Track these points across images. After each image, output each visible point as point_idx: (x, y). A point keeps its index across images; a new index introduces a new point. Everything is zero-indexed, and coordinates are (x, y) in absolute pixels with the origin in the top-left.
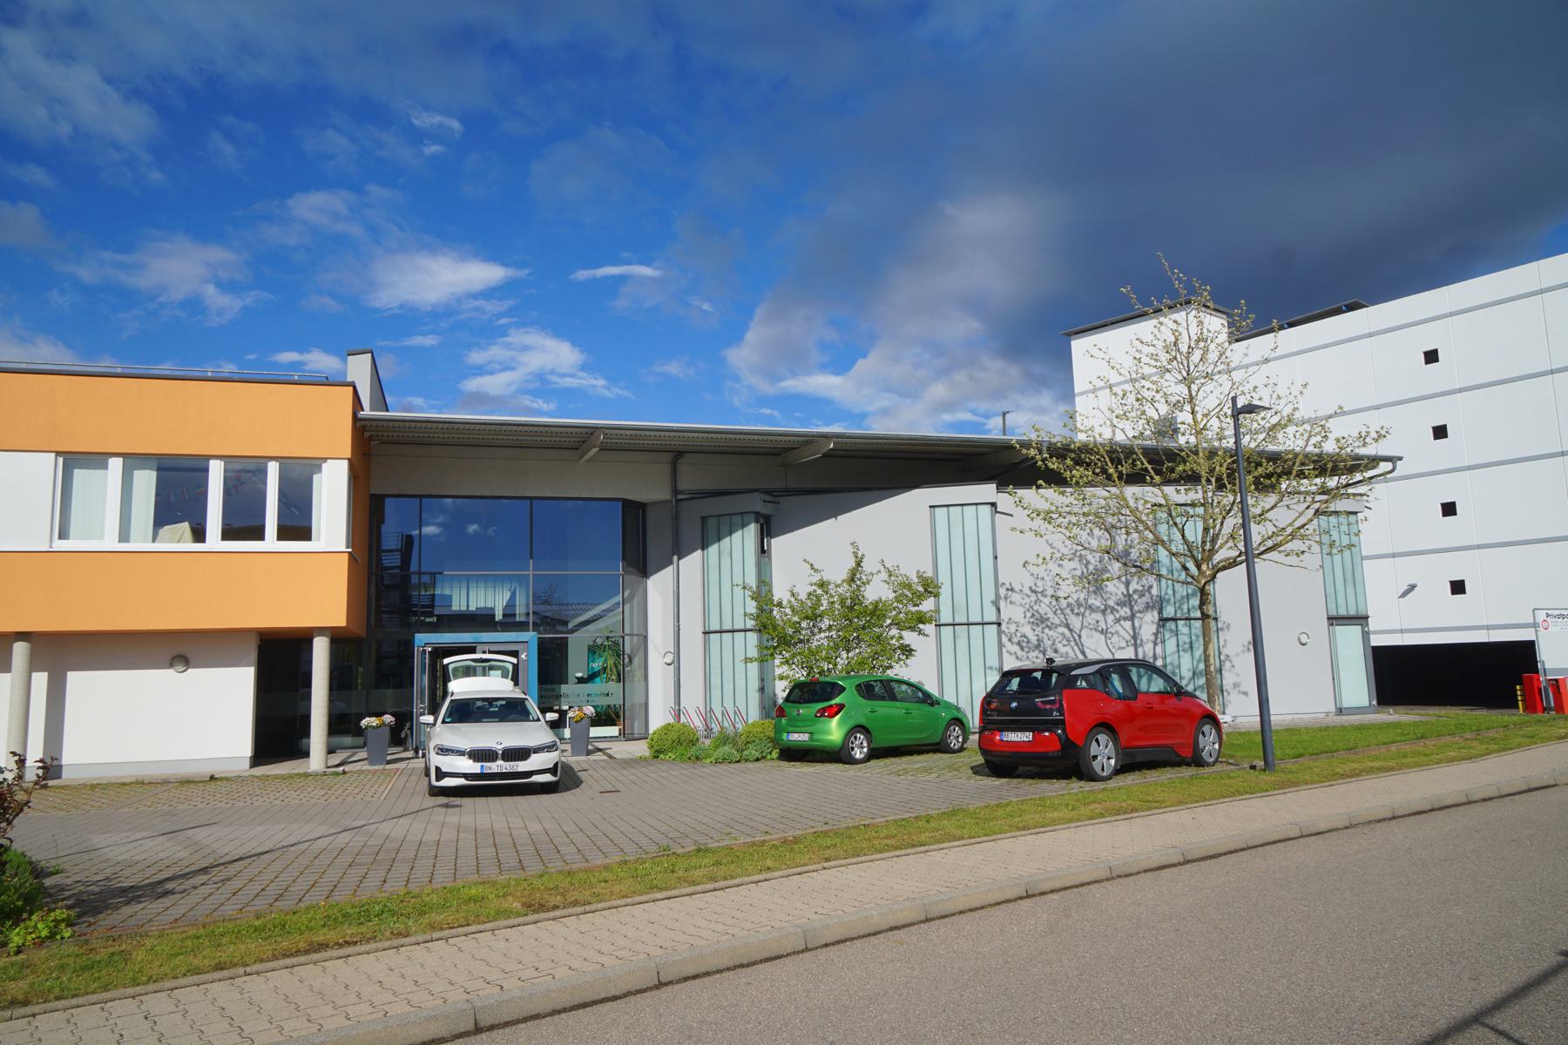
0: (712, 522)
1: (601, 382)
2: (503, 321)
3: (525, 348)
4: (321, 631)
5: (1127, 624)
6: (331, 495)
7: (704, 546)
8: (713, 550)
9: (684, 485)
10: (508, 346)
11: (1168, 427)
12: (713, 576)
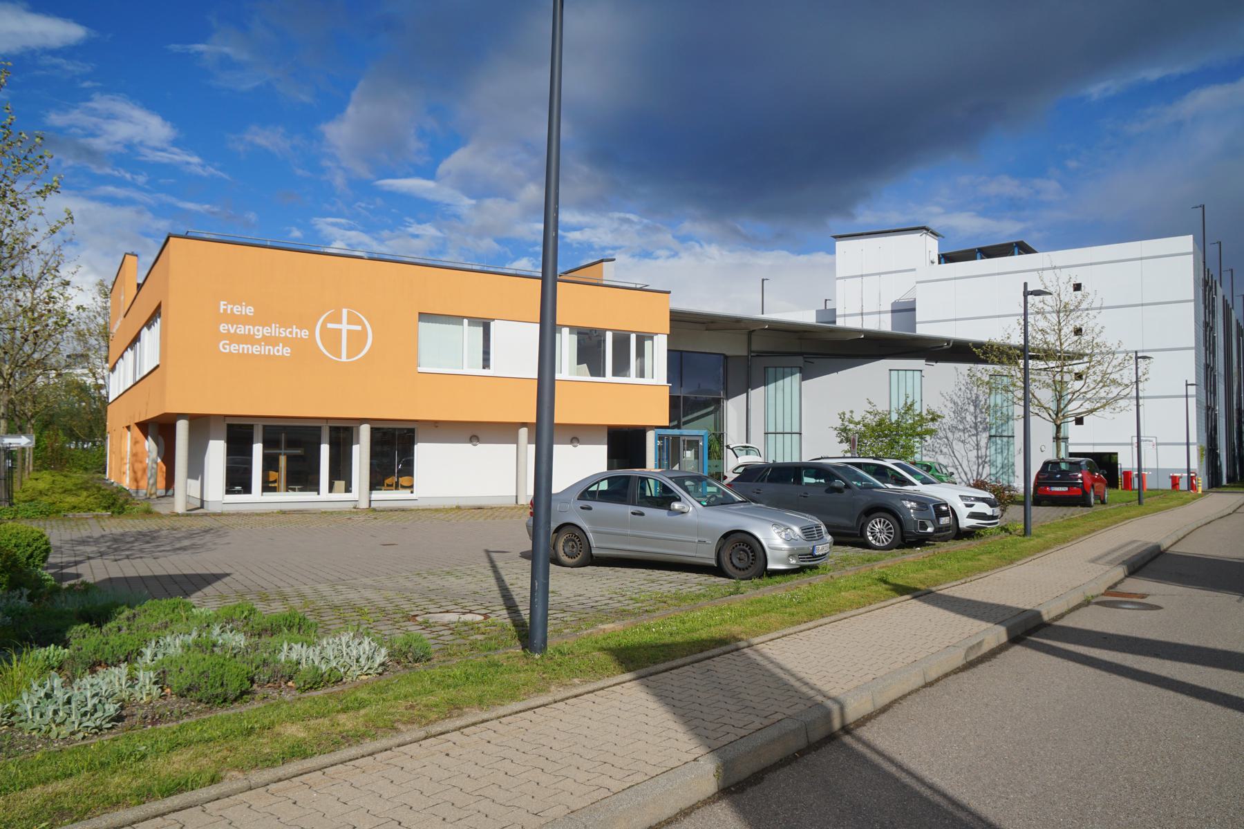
0: (771, 371)
1: (195, 160)
2: (87, 84)
3: (112, 117)
4: (524, 425)
5: (974, 438)
6: (659, 350)
7: (766, 384)
8: (771, 386)
9: (754, 348)
10: (93, 112)
11: (905, 310)
12: (771, 401)
